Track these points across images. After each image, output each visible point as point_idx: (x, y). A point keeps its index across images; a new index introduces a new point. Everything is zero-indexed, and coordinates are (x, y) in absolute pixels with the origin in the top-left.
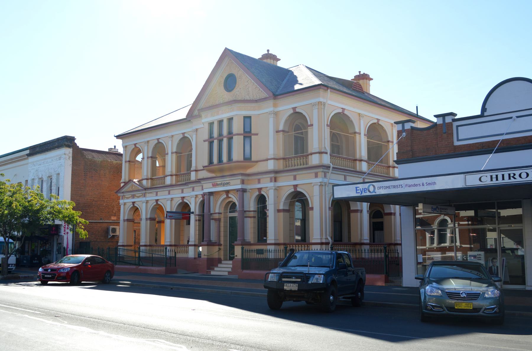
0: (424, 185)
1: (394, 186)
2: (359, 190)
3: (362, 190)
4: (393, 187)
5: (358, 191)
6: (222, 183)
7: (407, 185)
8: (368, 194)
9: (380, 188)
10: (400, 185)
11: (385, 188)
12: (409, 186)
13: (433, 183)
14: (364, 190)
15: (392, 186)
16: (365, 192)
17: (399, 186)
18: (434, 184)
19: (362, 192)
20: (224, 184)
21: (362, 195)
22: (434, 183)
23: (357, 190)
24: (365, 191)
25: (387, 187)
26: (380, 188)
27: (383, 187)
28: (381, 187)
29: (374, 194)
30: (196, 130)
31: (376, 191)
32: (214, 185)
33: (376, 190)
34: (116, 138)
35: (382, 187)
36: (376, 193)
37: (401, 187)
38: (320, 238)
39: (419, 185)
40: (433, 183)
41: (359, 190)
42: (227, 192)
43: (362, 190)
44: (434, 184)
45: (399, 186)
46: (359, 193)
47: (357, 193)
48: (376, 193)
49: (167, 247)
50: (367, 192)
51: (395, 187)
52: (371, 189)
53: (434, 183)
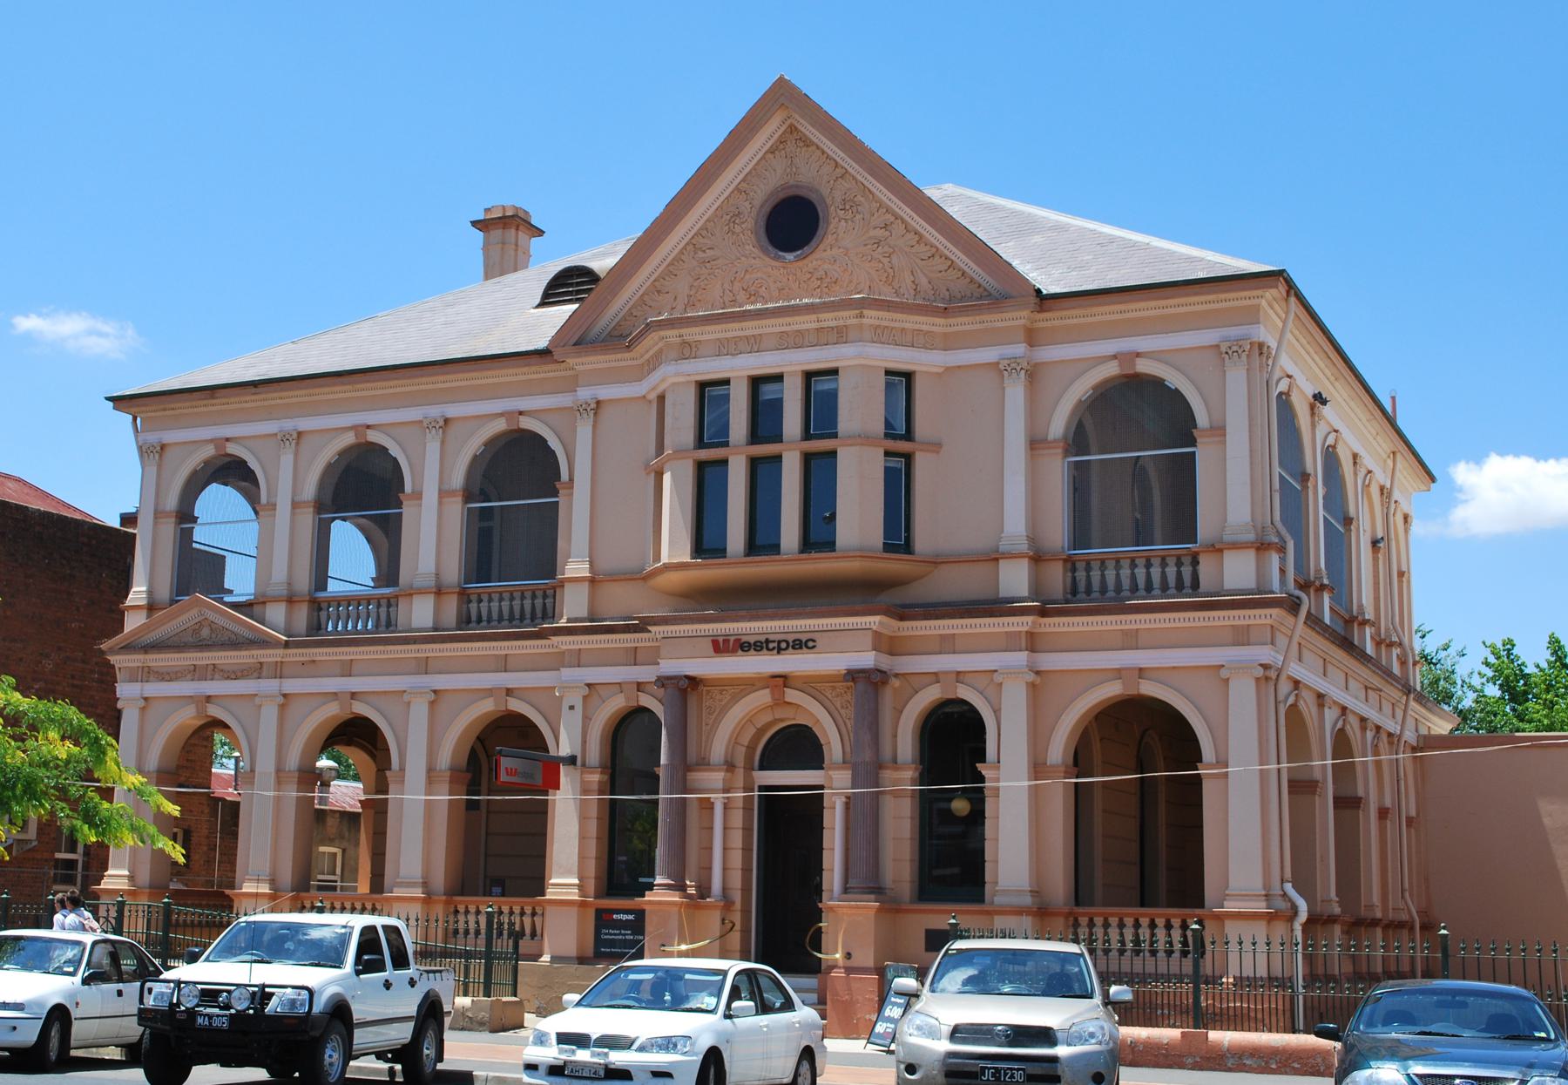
6: (767, 641)
20: (783, 645)
30: (593, 406)
32: (722, 646)
34: (111, 404)
42: (782, 681)
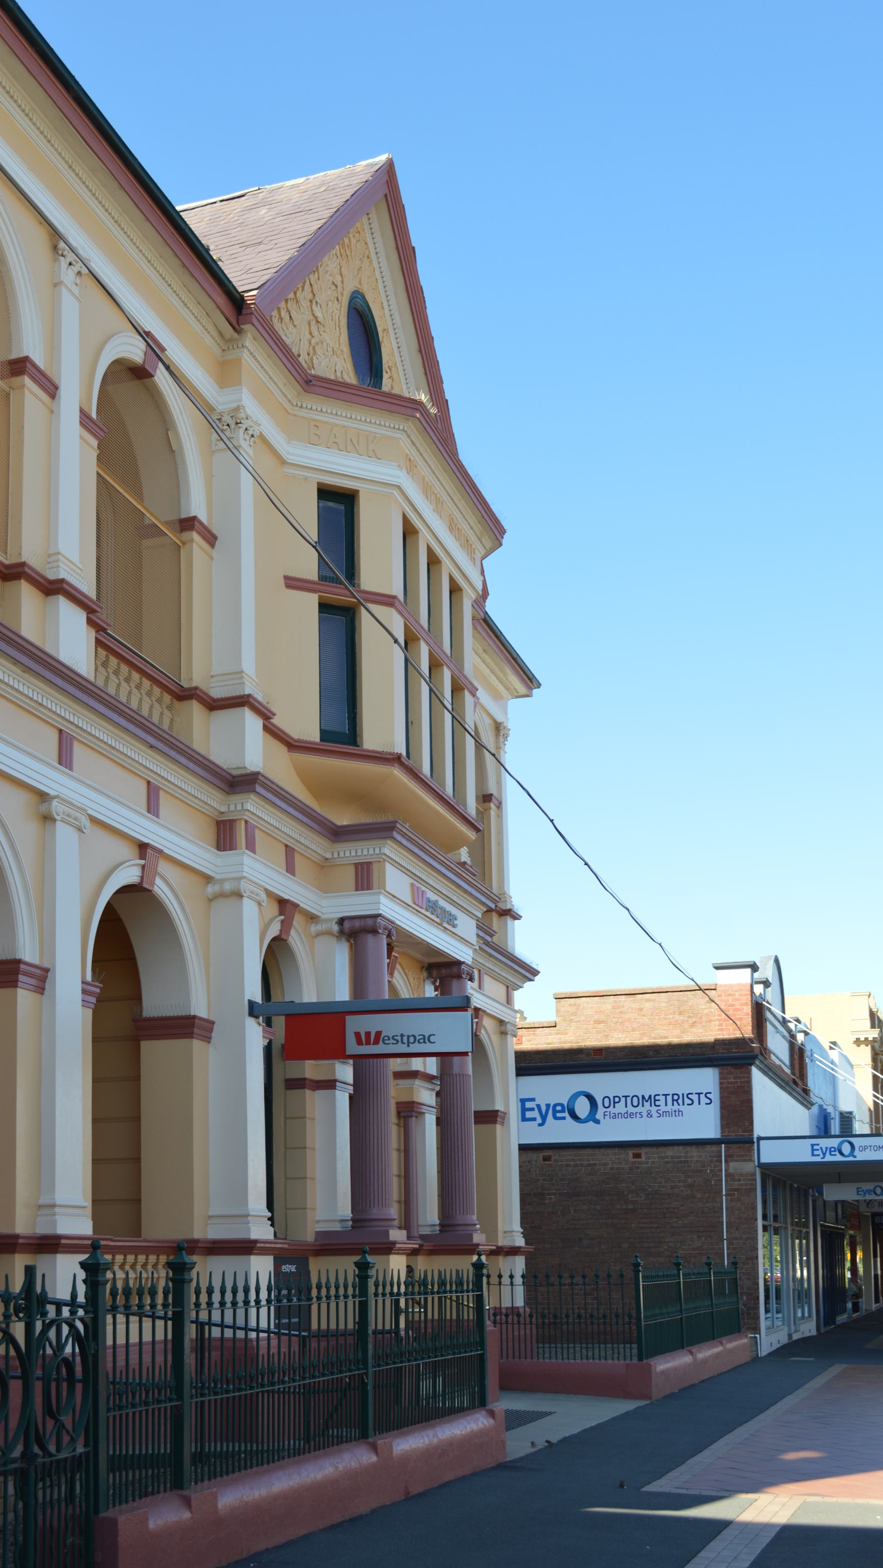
0: (651, 1116)
1: (676, 1097)
2: (532, 1109)
3: (544, 1109)
4: (669, 1098)
5: (816, 1153)
7: (608, 1113)
8: (838, 1158)
9: (865, 1148)
10: (699, 1094)
11: (635, 1103)
12: (612, 1115)
13: (675, 1111)
14: (830, 1151)
15: (666, 1095)
16: (831, 1155)
17: (695, 1097)
18: (677, 1114)
19: (824, 1155)
21: (826, 1160)
22: (677, 1113)
23: (813, 1150)
24: (833, 1153)
25: (643, 1097)
26: (865, 1148)
27: (629, 1099)
28: (617, 1100)
29: (851, 1159)
31: (855, 1154)
33: (856, 1153)
35: (626, 1097)
36: (855, 1157)
37: (704, 1100)
38: (503, 1306)
39: (638, 1114)
40: (675, 1111)
41: (532, 1109)
43: (544, 1109)
44: (677, 1114)
45: (695, 1097)
46: (819, 1155)
47: (813, 1155)
48: (855, 1157)
49: (370, 1259)
50: (835, 1155)
51: (680, 1101)
52: (846, 1149)
53: (677, 1113)
